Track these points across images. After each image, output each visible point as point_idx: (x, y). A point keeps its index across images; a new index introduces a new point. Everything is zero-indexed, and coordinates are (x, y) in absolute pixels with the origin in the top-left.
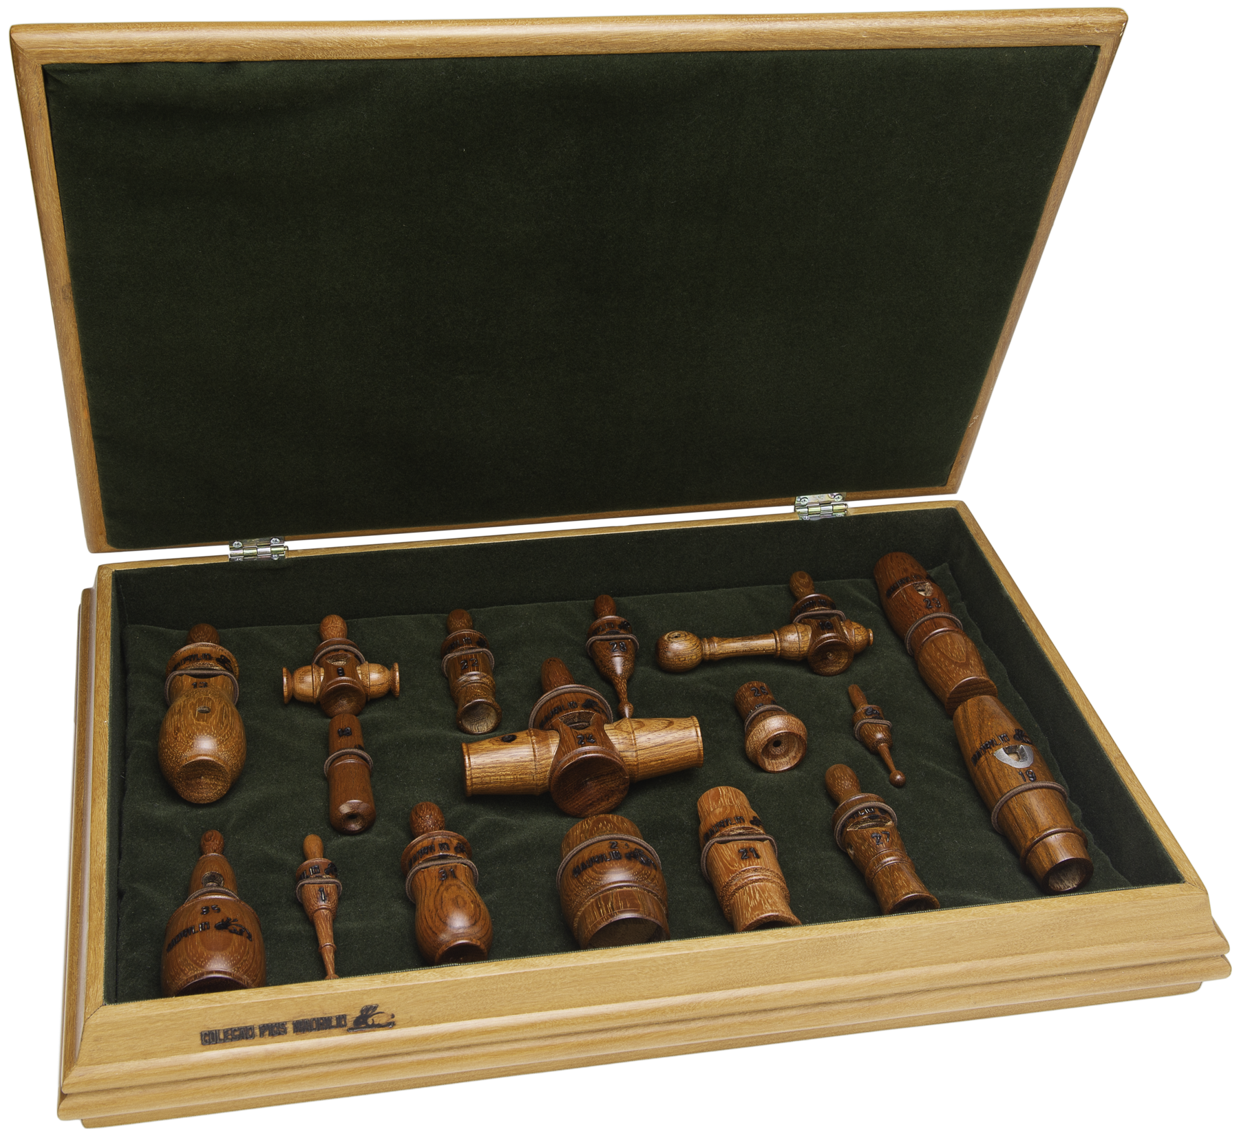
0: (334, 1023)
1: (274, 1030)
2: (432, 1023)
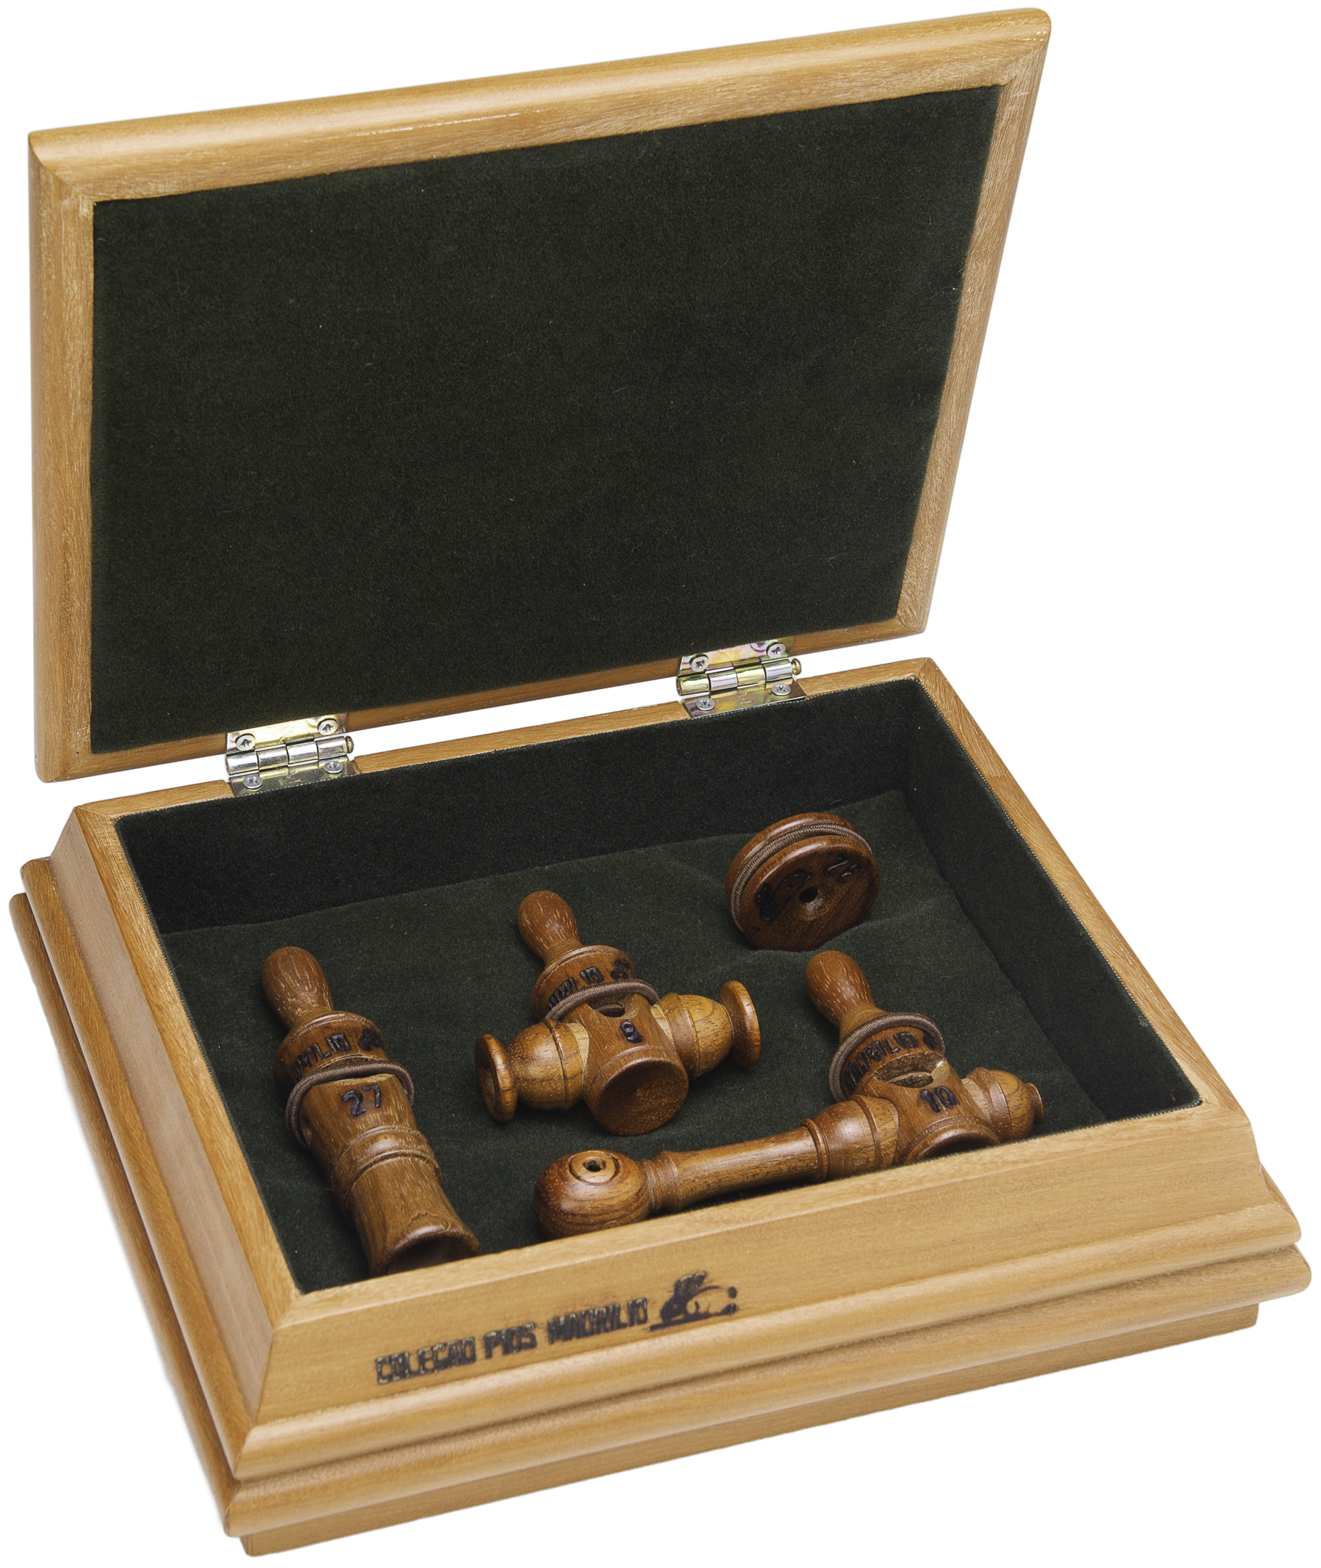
0: (624, 1317)
1: (513, 1341)
2: (308, 1410)
